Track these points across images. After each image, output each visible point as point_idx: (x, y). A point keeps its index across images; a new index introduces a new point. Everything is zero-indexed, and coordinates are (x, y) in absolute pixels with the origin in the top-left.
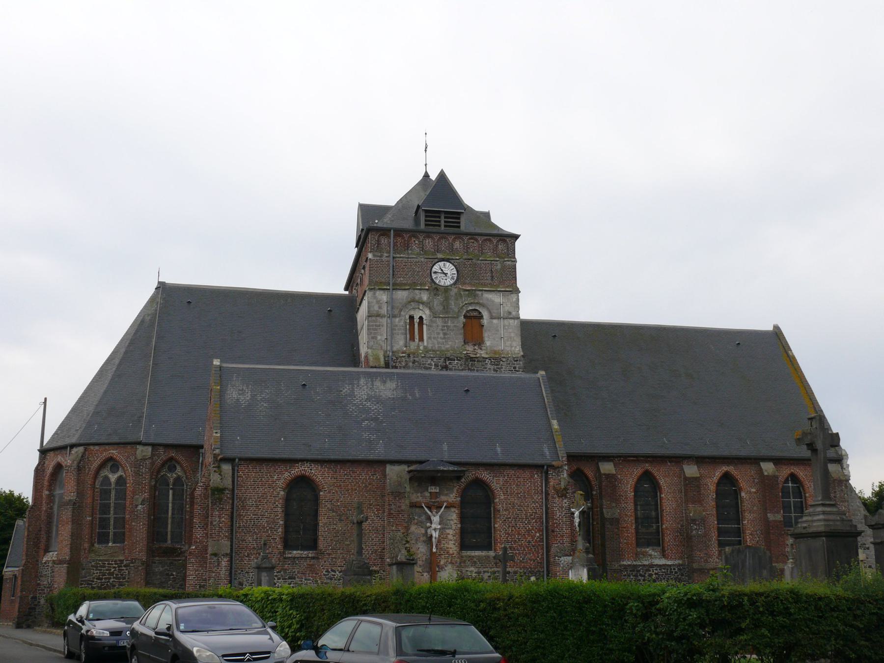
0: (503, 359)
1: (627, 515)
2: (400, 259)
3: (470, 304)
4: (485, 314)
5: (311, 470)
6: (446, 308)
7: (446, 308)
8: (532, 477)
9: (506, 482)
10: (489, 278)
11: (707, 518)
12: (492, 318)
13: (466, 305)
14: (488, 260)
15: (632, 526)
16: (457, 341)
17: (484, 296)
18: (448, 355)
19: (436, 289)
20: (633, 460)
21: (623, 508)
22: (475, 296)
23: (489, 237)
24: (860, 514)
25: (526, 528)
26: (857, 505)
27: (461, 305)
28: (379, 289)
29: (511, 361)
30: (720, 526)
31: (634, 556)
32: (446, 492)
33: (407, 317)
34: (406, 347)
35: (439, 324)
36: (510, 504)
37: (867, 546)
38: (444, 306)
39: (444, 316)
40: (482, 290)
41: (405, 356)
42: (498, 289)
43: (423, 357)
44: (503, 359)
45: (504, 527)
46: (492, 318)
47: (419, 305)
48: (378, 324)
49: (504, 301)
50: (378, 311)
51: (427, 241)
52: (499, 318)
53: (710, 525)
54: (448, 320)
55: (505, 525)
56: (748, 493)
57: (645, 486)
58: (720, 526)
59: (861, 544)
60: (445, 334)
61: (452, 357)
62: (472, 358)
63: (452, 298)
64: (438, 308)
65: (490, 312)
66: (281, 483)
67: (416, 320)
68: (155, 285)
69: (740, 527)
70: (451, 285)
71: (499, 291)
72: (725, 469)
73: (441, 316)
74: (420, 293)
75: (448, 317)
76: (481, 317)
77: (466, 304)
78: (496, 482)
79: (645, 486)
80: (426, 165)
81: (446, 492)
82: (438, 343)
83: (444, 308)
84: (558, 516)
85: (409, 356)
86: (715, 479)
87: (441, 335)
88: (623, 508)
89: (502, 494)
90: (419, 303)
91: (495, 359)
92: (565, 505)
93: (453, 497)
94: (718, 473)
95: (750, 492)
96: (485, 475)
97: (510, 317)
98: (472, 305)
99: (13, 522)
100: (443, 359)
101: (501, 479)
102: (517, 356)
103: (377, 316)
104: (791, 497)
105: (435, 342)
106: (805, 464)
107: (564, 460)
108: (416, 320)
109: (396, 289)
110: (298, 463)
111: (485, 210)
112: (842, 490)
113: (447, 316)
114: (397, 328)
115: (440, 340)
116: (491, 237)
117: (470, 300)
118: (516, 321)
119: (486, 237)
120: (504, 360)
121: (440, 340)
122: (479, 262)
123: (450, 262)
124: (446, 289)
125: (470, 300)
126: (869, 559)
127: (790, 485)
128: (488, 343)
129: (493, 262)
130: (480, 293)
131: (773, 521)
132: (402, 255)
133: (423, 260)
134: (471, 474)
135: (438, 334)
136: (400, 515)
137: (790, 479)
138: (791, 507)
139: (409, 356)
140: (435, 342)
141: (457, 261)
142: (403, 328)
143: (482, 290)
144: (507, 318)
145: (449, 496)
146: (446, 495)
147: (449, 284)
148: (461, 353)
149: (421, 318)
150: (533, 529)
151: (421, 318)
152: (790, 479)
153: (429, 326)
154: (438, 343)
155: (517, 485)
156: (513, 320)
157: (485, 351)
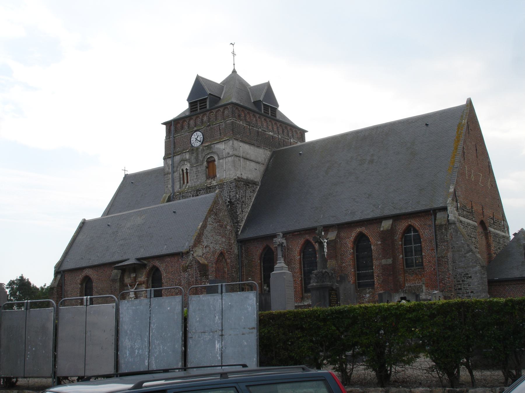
0: (224, 184)
1: (295, 272)
2: (178, 137)
3: (208, 154)
4: (216, 158)
5: (89, 272)
6: (197, 159)
7: (197, 159)
8: (178, 260)
9: (166, 265)
10: (219, 135)
11: (347, 268)
12: (219, 159)
13: (206, 155)
14: (218, 123)
15: (298, 279)
16: (203, 179)
17: (215, 147)
18: (198, 188)
19: (193, 150)
20: (298, 234)
21: (293, 267)
22: (211, 148)
23: (218, 109)
24: (464, 250)
25: (175, 292)
26: (462, 243)
27: (204, 155)
28: (167, 158)
29: (229, 184)
30: (372, 271)
31: (300, 299)
32: (140, 276)
33: (181, 170)
34: (180, 188)
35: (194, 171)
36: (168, 279)
37: (470, 275)
38: (196, 159)
39: (196, 165)
40: (214, 144)
41: (178, 194)
42: (222, 141)
43: (186, 193)
44: (224, 184)
45: (166, 292)
46: (219, 159)
47: (185, 162)
48: (168, 178)
49: (225, 147)
50: (168, 171)
51: (192, 121)
52: (223, 158)
53: (349, 273)
54: (198, 167)
55: (166, 291)
56: (375, 244)
57: (310, 250)
58: (372, 271)
59: (464, 274)
60: (197, 176)
61: (200, 189)
62: (209, 187)
63: (200, 153)
64: (193, 161)
65: (218, 156)
66: (79, 281)
67: (185, 171)
68: (123, 176)
69: (358, 271)
70: (200, 145)
71: (222, 141)
72: (358, 230)
73: (195, 165)
74: (185, 155)
75: (198, 165)
76: (214, 161)
77: (206, 155)
78: (161, 266)
79: (310, 250)
80: (234, 64)
81: (140, 276)
82: (194, 182)
83: (196, 161)
84: (183, 283)
85: (180, 194)
86: (352, 239)
87: (195, 177)
88: (293, 267)
89: (165, 273)
90: (185, 160)
91: (221, 184)
92: (186, 276)
93: (142, 278)
94: (354, 234)
95: (377, 244)
96: (157, 263)
97: (229, 155)
98: (209, 154)
99: (254, 290)
100: (196, 191)
101: (164, 264)
102: (231, 180)
103: (167, 174)
104: (413, 243)
105: (193, 181)
106: (420, 216)
107: (191, 248)
108: (185, 171)
109: (175, 156)
110: (84, 270)
111: (265, 81)
112: (442, 233)
113: (197, 165)
114: (176, 178)
115: (195, 180)
116: (219, 108)
117: (208, 151)
118: (232, 157)
119: (217, 109)
120: (225, 184)
121: (195, 180)
122: (214, 126)
123: (199, 131)
124: (197, 148)
125: (208, 151)
126: (471, 286)
127: (412, 234)
128: (218, 176)
129: (220, 124)
130: (213, 146)
131: (384, 265)
132: (178, 135)
133: (187, 134)
134: (150, 265)
135: (194, 176)
136: (116, 292)
137: (412, 229)
138: (412, 252)
139: (180, 194)
140: (193, 181)
141: (203, 129)
142: (178, 178)
143: (214, 144)
144: (227, 157)
145: (142, 278)
146: (141, 277)
147: (199, 145)
148: (204, 185)
149: (187, 169)
150: (178, 292)
151: (187, 169)
152: (412, 229)
153: (190, 173)
154: (194, 182)
155: (172, 267)
156: (230, 158)
157: (216, 181)
